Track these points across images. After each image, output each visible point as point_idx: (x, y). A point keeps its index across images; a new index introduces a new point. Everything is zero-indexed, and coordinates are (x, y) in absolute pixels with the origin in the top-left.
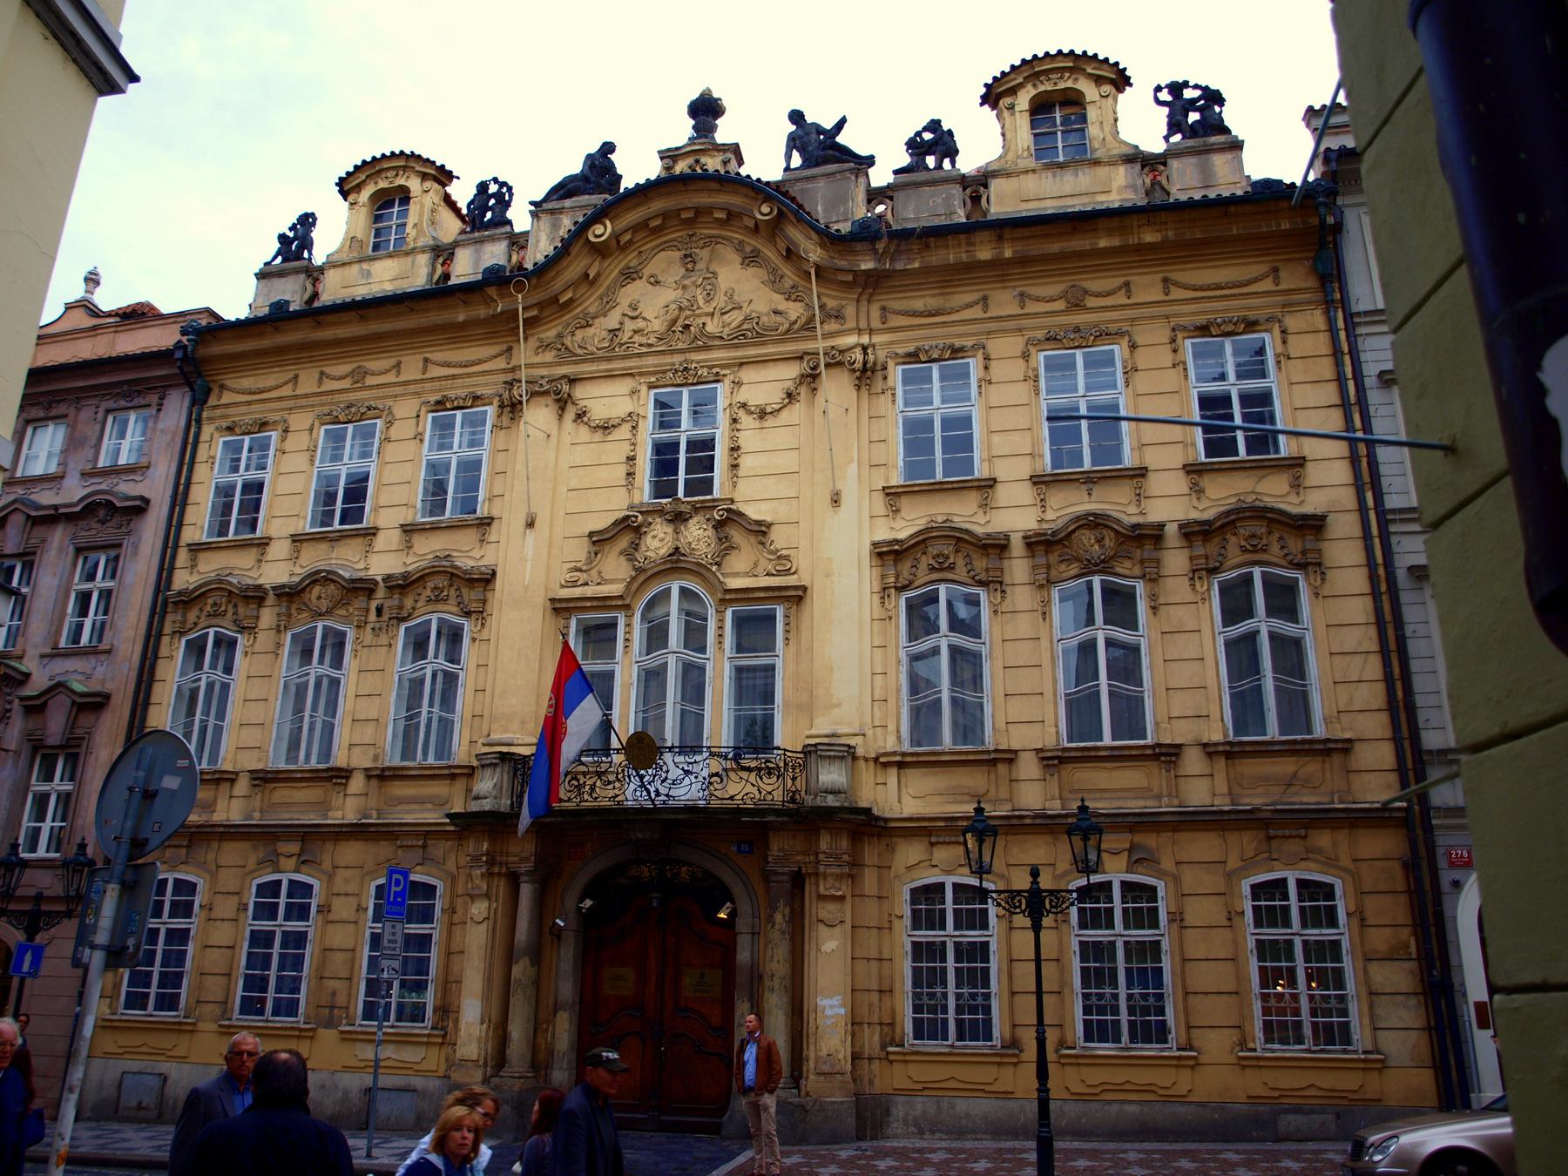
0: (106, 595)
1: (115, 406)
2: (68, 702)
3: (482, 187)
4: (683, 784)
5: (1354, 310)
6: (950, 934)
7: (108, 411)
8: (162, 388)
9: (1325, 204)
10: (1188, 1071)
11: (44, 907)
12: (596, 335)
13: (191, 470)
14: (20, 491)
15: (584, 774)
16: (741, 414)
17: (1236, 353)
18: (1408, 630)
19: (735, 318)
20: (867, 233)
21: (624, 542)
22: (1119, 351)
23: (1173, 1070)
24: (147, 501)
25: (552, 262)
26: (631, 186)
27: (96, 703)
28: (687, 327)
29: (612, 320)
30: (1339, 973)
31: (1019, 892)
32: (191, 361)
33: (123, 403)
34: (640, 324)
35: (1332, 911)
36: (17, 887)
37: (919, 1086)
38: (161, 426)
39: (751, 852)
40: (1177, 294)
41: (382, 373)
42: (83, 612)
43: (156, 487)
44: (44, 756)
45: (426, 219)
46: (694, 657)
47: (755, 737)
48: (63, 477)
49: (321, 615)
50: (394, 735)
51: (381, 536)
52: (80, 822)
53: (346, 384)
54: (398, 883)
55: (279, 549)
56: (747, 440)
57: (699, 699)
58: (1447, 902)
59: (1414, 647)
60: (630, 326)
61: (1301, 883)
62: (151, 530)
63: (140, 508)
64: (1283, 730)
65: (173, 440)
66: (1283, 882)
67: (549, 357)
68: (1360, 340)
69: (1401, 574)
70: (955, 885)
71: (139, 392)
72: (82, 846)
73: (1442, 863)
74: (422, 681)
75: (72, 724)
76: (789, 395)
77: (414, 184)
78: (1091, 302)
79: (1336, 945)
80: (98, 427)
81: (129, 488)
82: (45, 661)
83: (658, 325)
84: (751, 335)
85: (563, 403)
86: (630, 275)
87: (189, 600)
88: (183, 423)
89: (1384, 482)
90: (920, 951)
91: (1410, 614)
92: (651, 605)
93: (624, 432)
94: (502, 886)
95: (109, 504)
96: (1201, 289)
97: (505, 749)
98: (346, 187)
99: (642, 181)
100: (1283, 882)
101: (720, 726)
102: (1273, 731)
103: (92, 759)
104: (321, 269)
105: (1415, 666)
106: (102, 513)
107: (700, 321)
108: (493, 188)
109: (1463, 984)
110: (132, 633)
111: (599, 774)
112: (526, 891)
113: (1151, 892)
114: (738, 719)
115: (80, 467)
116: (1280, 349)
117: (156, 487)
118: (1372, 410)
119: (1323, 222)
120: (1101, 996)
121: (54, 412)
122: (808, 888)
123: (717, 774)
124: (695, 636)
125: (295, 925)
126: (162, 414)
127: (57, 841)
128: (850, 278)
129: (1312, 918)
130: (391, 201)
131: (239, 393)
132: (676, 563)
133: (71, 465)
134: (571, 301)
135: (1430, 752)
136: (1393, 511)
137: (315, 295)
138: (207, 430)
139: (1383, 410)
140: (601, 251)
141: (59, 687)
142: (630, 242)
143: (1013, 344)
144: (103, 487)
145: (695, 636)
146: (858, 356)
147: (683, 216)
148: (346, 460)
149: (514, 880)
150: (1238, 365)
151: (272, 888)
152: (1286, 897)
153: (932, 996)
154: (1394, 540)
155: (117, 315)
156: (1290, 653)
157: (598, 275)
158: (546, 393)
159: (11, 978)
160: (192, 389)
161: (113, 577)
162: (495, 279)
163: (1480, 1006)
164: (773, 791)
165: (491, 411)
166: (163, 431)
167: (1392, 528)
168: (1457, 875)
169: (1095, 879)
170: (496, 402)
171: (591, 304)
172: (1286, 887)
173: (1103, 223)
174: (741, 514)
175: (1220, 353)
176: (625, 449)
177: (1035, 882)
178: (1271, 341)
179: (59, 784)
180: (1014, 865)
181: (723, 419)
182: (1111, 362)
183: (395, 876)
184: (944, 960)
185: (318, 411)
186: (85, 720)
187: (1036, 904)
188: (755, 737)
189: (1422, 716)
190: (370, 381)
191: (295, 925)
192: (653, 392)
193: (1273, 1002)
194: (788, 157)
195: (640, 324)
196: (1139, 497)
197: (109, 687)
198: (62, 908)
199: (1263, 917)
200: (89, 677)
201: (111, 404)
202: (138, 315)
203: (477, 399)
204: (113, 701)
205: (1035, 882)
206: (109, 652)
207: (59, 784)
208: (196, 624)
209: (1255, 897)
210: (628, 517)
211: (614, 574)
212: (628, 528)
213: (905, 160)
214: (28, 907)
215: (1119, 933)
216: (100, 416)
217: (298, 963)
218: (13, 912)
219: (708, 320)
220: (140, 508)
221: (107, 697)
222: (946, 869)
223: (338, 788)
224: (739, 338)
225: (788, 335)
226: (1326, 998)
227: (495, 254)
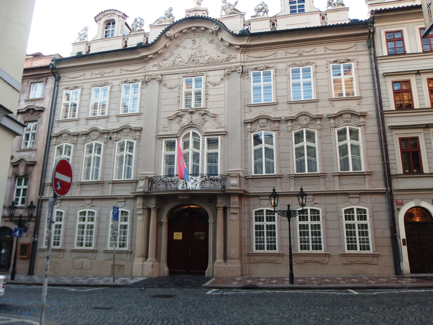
0: (34, 135)
1: (33, 82)
2: (25, 164)
3: (136, 21)
4: (193, 184)
5: (377, 56)
6: (356, 222)
7: (32, 83)
8: (47, 76)
9: (371, 26)
10: (376, 258)
11: (23, 219)
12: (168, 63)
13: (56, 100)
14: (31, 104)
15: (168, 182)
16: (209, 84)
17: (344, 68)
18: (388, 143)
19: (207, 58)
20: (244, 34)
21: (177, 120)
22: (312, 67)
23: (323, 257)
24: (44, 108)
25: (156, 41)
26: (178, 20)
27: (33, 164)
28: (194, 60)
29: (173, 58)
30: (367, 232)
31: (285, 211)
32: (53, 70)
33: (35, 81)
34: (181, 59)
35: (318, 217)
36: (14, 214)
37: (350, 263)
38: (47, 87)
39: (211, 202)
40: (328, 52)
41: (347, 49)
42: (27, 139)
43: (46, 104)
44: (19, 179)
45: (118, 28)
46: (196, 150)
47: (212, 171)
48: (44, 99)
49: (95, 140)
50: (116, 172)
51: (111, 118)
52: (30, 196)
53: (99, 76)
54: (116, 211)
55: (83, 122)
56: (210, 92)
57: (198, 161)
58: (396, 214)
59: (389, 148)
60: (178, 60)
61: (358, 209)
62: (45, 116)
63: (42, 111)
64: (309, 171)
65: (50, 91)
66: (353, 209)
67: (156, 68)
68: (378, 64)
69: (387, 128)
70: (266, 210)
71: (40, 78)
72: (32, 202)
73: (395, 204)
74: (91, 158)
75: (26, 170)
76: (222, 79)
77: (116, 18)
78: (106, 75)
79: (319, 225)
80: (29, 88)
81: (38, 105)
82: (18, 153)
83: (186, 60)
84: (212, 62)
85: (160, 81)
86: (177, 46)
87: (59, 136)
88: (53, 86)
89: (383, 103)
90: (348, 226)
91: (389, 139)
92: (184, 138)
93: (176, 90)
94: (146, 211)
95: (33, 109)
96: (335, 50)
97: (146, 175)
98: (97, 19)
99: (181, 19)
100: (353, 209)
101: (204, 169)
102: (351, 170)
103: (32, 179)
104: (91, 43)
105: (389, 152)
106: (31, 111)
107: (197, 58)
108: (139, 20)
109: (399, 235)
110: (42, 145)
111: (172, 182)
112: (153, 214)
113: (365, 211)
114: (166, 169)
115: (24, 99)
116: (356, 67)
117: (46, 104)
118: (380, 83)
119: (370, 31)
120: (305, 239)
121: (39, 81)
122: (228, 210)
123: (203, 181)
124: (196, 144)
125: (90, 223)
126: (47, 84)
127: (23, 201)
128: (239, 47)
129: (314, 218)
130: (110, 23)
131: (67, 79)
132: (191, 126)
133: (22, 98)
134: (161, 53)
135: (393, 175)
136: (385, 111)
137: (89, 50)
138: (61, 88)
139: (384, 84)
140: (170, 38)
141: (21, 160)
142: (178, 36)
143: (324, 62)
144: (31, 104)
145: (196, 144)
146: (241, 68)
147: (192, 29)
148: (130, 94)
149: (149, 210)
150: (344, 71)
151: (84, 213)
152: (353, 213)
153: (260, 239)
154: (385, 119)
155: (32, 55)
156: (312, 151)
157: (169, 45)
158: (155, 79)
159: (13, 238)
160: (55, 77)
161: (35, 129)
162: (141, 47)
163: (403, 240)
164: (218, 186)
165: (140, 84)
166: (47, 89)
167: (385, 116)
168: (399, 207)
169: (305, 208)
170: (141, 81)
171: (168, 55)
172: (353, 210)
173: (63, 61)
174: (208, 112)
175: (339, 68)
176: (177, 94)
177: (289, 209)
178: (353, 65)
179: (23, 187)
180: (282, 204)
181: (203, 85)
182: (270, 74)
183: (115, 209)
184: (263, 229)
185: (328, 60)
186: (30, 169)
187: (289, 214)
188: (212, 171)
189: (391, 166)
190: (106, 75)
191: (90, 223)
192: (184, 78)
193: (259, 240)
194: (222, 12)
195: (181, 59)
196: (317, 107)
197: (36, 160)
198: (27, 219)
199: (348, 218)
200: (30, 157)
201: (32, 81)
202: (37, 56)
203: (136, 81)
204: (37, 164)
205: (289, 209)
206: (35, 150)
207: (23, 187)
208: (60, 142)
209: (345, 213)
210: (178, 113)
211: (175, 128)
212: (179, 116)
213: (254, 13)
214: (18, 219)
215: (356, 222)
216: (29, 84)
217: (91, 233)
218: (14, 220)
219: (199, 58)
220: (42, 111)
221: (36, 162)
222: (266, 206)
223: (101, 186)
224: (208, 64)
225: (221, 63)
226: (363, 239)
227: (140, 39)
